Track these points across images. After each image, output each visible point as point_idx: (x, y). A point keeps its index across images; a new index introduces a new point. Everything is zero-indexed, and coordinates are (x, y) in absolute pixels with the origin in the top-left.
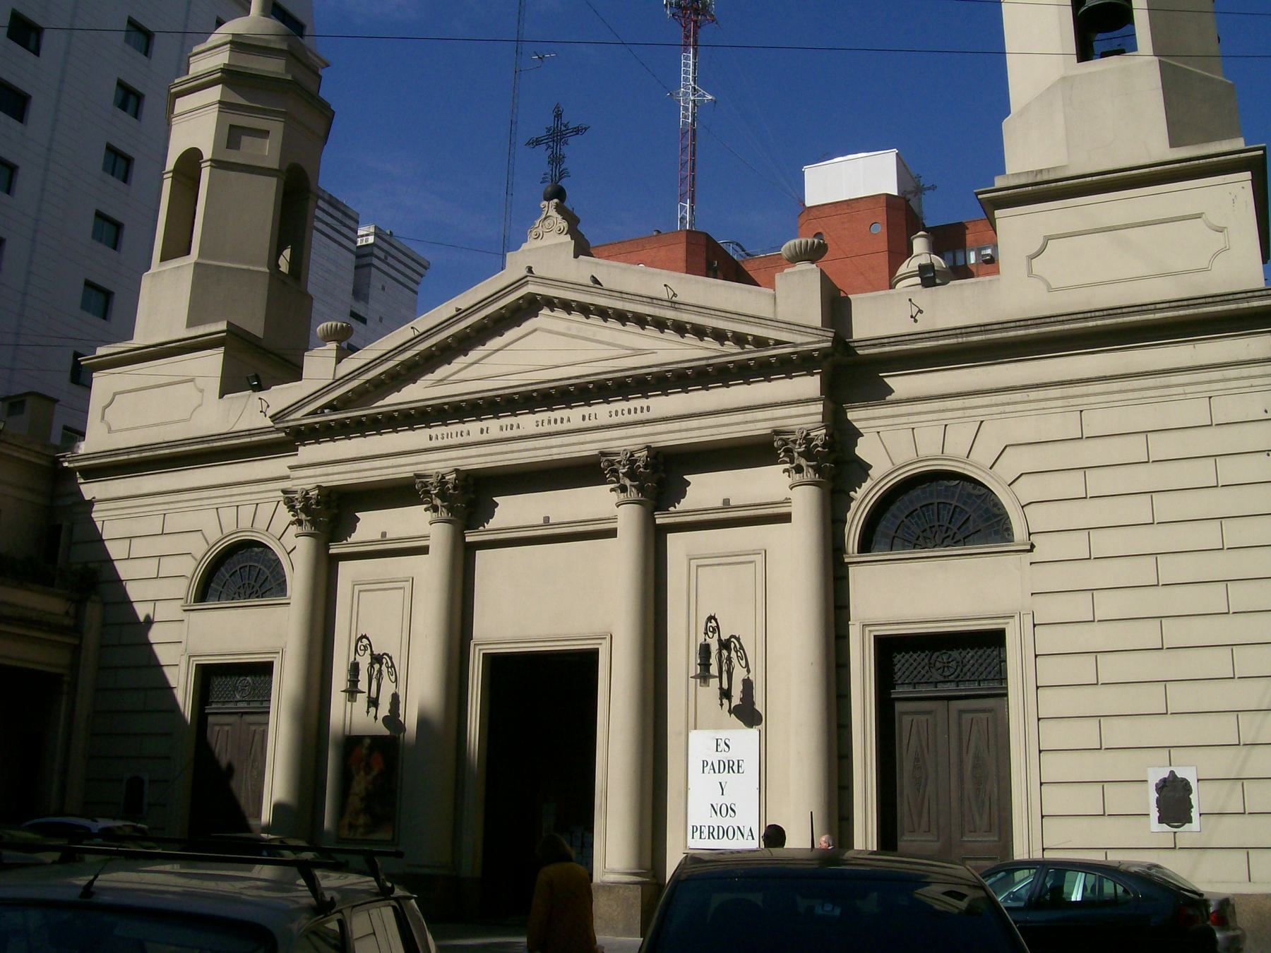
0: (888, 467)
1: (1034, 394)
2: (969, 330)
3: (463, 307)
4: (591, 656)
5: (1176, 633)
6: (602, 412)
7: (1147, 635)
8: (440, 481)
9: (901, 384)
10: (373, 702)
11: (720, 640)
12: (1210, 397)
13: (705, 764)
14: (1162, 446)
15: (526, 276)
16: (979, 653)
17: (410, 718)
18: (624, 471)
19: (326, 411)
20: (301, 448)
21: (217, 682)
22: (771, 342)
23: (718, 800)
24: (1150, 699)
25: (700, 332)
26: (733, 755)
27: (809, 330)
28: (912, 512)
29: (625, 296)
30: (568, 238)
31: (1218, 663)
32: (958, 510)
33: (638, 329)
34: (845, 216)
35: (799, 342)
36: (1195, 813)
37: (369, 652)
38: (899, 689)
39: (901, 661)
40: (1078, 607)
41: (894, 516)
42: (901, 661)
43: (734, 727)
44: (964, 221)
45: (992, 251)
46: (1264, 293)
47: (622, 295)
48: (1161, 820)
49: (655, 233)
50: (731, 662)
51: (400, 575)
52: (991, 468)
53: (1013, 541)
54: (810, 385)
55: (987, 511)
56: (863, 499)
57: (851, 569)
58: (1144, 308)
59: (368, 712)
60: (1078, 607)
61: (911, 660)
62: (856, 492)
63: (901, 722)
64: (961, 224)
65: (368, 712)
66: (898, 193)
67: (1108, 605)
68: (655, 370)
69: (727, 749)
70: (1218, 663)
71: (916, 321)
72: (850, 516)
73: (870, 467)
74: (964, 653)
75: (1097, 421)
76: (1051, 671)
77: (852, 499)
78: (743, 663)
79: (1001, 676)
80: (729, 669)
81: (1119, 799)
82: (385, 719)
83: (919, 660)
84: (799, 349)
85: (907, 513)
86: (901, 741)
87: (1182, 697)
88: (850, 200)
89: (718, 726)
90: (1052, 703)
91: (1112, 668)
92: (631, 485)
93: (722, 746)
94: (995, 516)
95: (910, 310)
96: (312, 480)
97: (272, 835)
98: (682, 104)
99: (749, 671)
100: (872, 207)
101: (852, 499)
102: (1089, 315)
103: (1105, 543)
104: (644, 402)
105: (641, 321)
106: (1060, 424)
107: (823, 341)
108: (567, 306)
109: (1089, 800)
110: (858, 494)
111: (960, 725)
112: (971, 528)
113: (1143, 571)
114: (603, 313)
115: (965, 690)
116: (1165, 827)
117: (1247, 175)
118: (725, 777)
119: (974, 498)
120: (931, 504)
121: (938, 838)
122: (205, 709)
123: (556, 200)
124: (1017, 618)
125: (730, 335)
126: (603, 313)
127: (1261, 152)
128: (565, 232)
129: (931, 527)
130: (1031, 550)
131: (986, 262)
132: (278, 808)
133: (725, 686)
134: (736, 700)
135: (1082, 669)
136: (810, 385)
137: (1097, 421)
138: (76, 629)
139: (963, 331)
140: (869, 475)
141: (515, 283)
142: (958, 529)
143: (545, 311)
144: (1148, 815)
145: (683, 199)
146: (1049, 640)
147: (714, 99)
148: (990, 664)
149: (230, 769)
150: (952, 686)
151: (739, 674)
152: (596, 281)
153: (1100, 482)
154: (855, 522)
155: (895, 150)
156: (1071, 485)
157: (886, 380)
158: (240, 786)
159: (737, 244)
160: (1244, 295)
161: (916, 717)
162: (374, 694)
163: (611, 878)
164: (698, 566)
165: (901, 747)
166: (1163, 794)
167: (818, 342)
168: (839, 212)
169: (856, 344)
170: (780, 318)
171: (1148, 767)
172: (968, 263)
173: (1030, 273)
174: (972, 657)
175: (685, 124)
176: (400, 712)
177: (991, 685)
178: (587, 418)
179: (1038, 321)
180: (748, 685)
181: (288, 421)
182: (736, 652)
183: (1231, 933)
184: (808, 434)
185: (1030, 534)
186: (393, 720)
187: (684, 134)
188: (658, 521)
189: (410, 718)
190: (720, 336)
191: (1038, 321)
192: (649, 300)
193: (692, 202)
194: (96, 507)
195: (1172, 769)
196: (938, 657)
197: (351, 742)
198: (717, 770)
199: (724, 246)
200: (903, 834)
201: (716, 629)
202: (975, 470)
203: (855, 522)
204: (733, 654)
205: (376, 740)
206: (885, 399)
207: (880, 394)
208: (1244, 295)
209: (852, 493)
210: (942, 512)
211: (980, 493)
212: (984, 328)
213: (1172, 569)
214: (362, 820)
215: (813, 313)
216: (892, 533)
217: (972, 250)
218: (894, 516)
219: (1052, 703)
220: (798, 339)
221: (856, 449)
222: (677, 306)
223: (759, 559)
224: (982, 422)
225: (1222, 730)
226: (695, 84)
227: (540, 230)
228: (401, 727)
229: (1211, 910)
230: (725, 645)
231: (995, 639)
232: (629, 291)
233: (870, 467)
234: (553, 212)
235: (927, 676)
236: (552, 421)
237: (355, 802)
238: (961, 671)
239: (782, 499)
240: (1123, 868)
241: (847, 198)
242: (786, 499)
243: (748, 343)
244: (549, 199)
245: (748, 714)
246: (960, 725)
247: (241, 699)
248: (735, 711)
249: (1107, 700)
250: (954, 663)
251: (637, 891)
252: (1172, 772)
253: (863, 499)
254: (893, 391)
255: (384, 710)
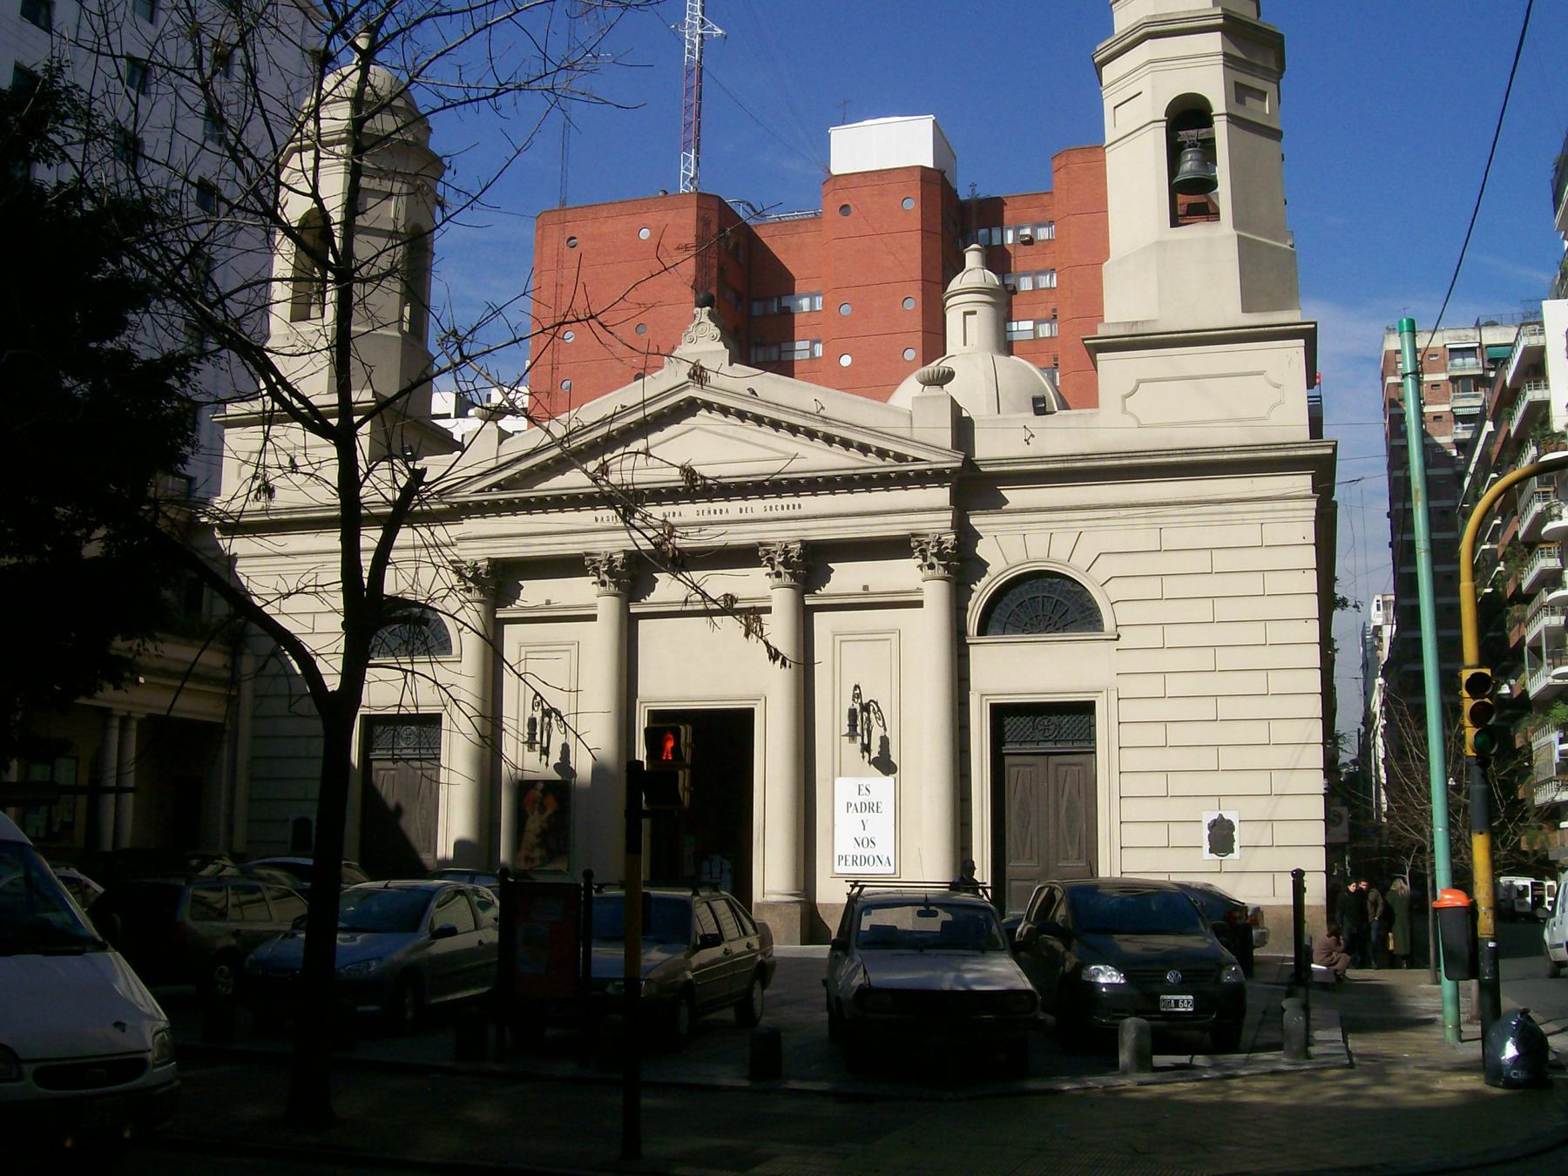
0: (1004, 566)
1: (1123, 512)
2: (1074, 458)
3: (629, 405)
4: (749, 714)
5: (1227, 708)
6: (757, 507)
7: (1205, 709)
8: (608, 560)
9: (1015, 496)
10: (545, 751)
11: (861, 704)
12: (1262, 524)
13: (849, 805)
14: (1223, 561)
15: (687, 382)
16: (1080, 719)
17: (583, 765)
18: (780, 560)
19: (494, 489)
20: (466, 521)
21: (379, 730)
22: (910, 459)
23: (861, 835)
24: (1206, 759)
25: (846, 444)
26: (872, 798)
27: (943, 452)
28: (1022, 603)
29: (781, 408)
30: (721, 346)
31: (1258, 733)
32: (1058, 603)
33: (790, 436)
34: (876, 187)
35: (934, 461)
36: (1236, 846)
37: (540, 707)
38: (1008, 746)
39: (1010, 723)
40: (1153, 686)
41: (1007, 605)
42: (1010, 723)
43: (877, 776)
44: (1002, 196)
45: (1031, 231)
46: (1308, 445)
47: (778, 406)
48: (1211, 851)
49: (661, 194)
50: (870, 722)
51: (566, 639)
52: (1087, 571)
53: (1103, 631)
54: (940, 495)
55: (1082, 605)
56: (982, 591)
57: (971, 648)
58: (1215, 450)
59: (541, 760)
60: (1153, 686)
61: (1018, 723)
62: (976, 585)
63: (1009, 772)
64: (999, 199)
65: (541, 760)
66: (935, 163)
67: (1177, 685)
68: (808, 475)
69: (867, 793)
70: (1258, 733)
71: (1028, 444)
72: (970, 604)
73: (988, 565)
74: (1062, 718)
75: (1173, 538)
76: (1130, 735)
77: (973, 591)
78: (881, 723)
79: (1091, 738)
80: (869, 727)
81: (1180, 835)
82: (556, 766)
83: (1025, 722)
84: (935, 466)
85: (1018, 603)
86: (1009, 788)
87: (1230, 758)
88: (881, 171)
89: (859, 774)
90: (1131, 760)
91: (1178, 734)
92: (785, 573)
93: (864, 791)
94: (1089, 609)
95: (1023, 434)
96: (486, 551)
97: (80, 871)
98: (687, 37)
99: (885, 730)
100: (906, 180)
101: (973, 591)
102: (1171, 452)
103: (1176, 636)
104: (796, 500)
105: (793, 429)
106: (1142, 537)
107: (954, 462)
108: (725, 411)
109: (1157, 835)
110: (978, 587)
111: (1057, 776)
112: (1069, 618)
113: (1204, 660)
114: (759, 420)
115: (1060, 747)
116: (1214, 856)
117: (1302, 342)
118: (866, 815)
119: (1072, 594)
120: (1037, 597)
121: (1038, 863)
122: (369, 755)
123: (708, 308)
124: (1105, 693)
125: (874, 449)
126: (759, 420)
127: (1313, 326)
128: (718, 339)
129: (1037, 616)
130: (1117, 640)
131: (1025, 243)
132: (460, 845)
133: (866, 742)
134: (875, 753)
135: (1155, 735)
136: (940, 495)
137: (1173, 538)
138: (233, 682)
139: (1069, 458)
140: (987, 571)
141: (681, 385)
142: (1059, 618)
143: (703, 412)
144: (1201, 847)
145: (686, 148)
146: (1129, 711)
147: (725, 33)
148: (1081, 728)
149: (399, 810)
150: (1050, 745)
151: (877, 732)
152: (753, 392)
153: (1174, 587)
154: (975, 611)
155: (932, 116)
156: (1151, 588)
157: (1002, 492)
158: (411, 826)
159: (748, 204)
160: (1292, 446)
161: (1021, 769)
162: (545, 745)
163: (775, 898)
164: (841, 641)
165: (1009, 792)
166: (1214, 830)
167: (951, 462)
168: (869, 183)
169: (980, 463)
170: (916, 439)
171: (1204, 810)
172: (1005, 243)
173: (1124, 409)
174: (1068, 722)
175: (690, 61)
176: (571, 759)
177: (1082, 745)
178: (744, 510)
179: (1130, 455)
180: (885, 741)
181: (456, 497)
182: (875, 713)
183: (1260, 931)
184: (940, 538)
185: (1117, 626)
186: (564, 766)
187: (689, 72)
188: (807, 603)
189: (583, 765)
190: (864, 449)
191: (1130, 455)
192: (803, 414)
193: (698, 152)
194: (239, 563)
195: (1220, 812)
196: (1040, 721)
197: (524, 788)
198: (859, 810)
199: (733, 206)
200: (1010, 862)
201: (859, 696)
202: (1073, 571)
203: (975, 611)
204: (872, 715)
205: (549, 785)
206: (1001, 508)
207: (997, 504)
208: (1292, 446)
209: (973, 586)
210: (1046, 604)
211: (1078, 590)
212: (1085, 457)
213: (1227, 659)
214: (537, 853)
215: (945, 438)
216: (1004, 619)
217: (1010, 228)
218: (1007, 605)
219: (1131, 760)
220: (933, 458)
221: (977, 549)
222: (827, 421)
223: (894, 637)
224: (1081, 532)
225: (1259, 783)
226: (703, 14)
227: (693, 334)
228: (573, 773)
229: (1249, 914)
230: (865, 708)
231: (1087, 709)
232: (784, 403)
233: (988, 565)
234: (705, 319)
235: (1031, 736)
236: (712, 512)
237: (530, 837)
238: (1059, 732)
239: (914, 588)
240: (1193, 886)
241: (878, 169)
242: (918, 588)
243: (889, 457)
244: (702, 306)
245: (885, 765)
246: (1057, 776)
247: (406, 746)
248: (874, 762)
249: (1172, 759)
250: (1053, 727)
251: (798, 908)
252: (1221, 815)
253: (982, 591)
254: (1008, 502)
255: (555, 757)
